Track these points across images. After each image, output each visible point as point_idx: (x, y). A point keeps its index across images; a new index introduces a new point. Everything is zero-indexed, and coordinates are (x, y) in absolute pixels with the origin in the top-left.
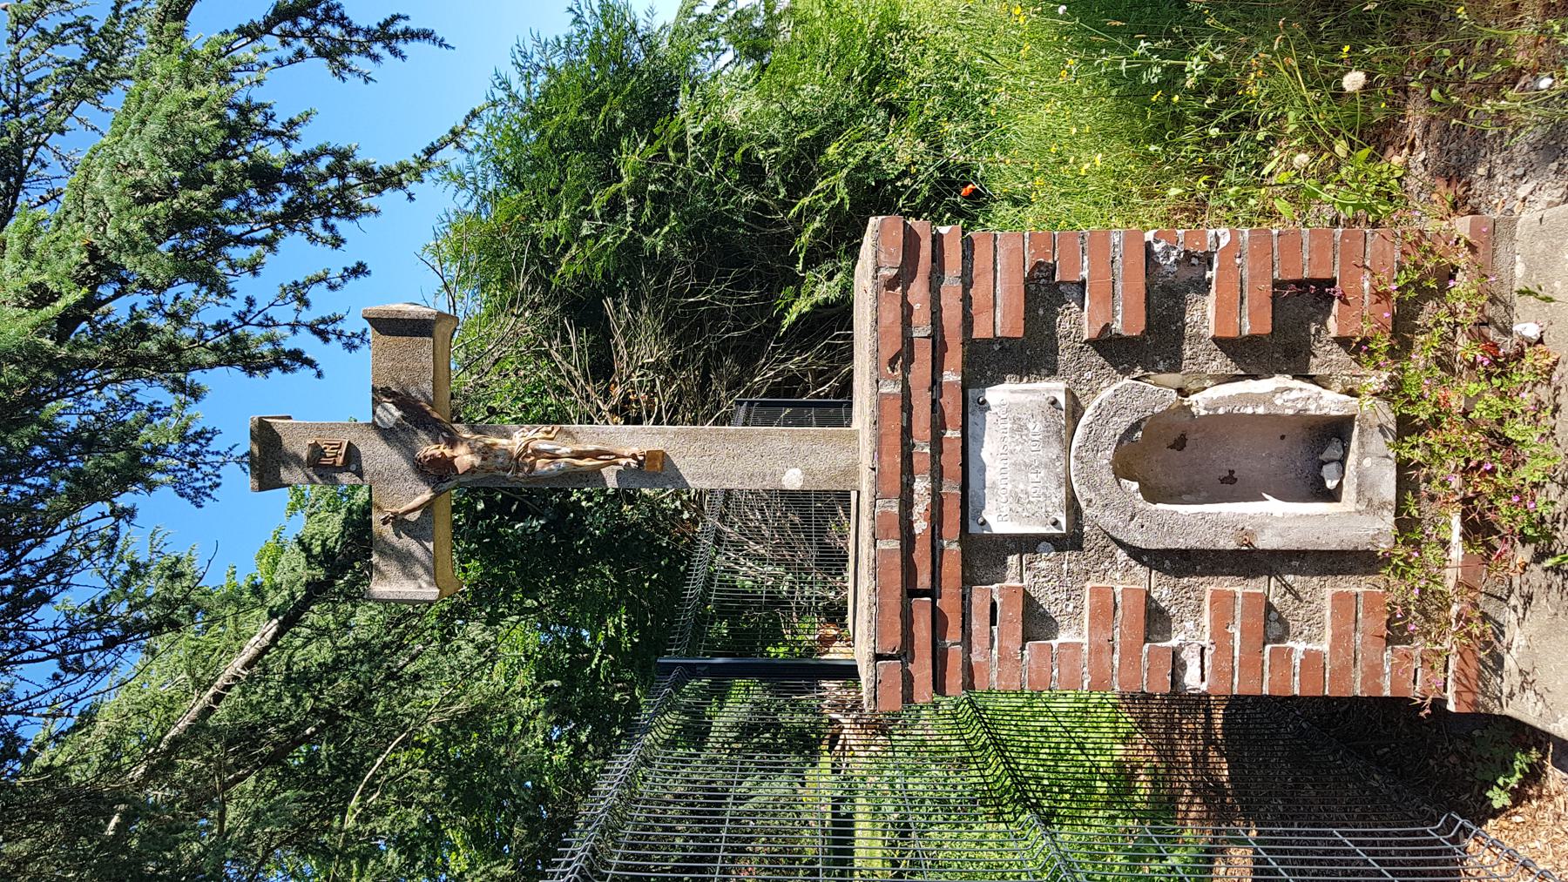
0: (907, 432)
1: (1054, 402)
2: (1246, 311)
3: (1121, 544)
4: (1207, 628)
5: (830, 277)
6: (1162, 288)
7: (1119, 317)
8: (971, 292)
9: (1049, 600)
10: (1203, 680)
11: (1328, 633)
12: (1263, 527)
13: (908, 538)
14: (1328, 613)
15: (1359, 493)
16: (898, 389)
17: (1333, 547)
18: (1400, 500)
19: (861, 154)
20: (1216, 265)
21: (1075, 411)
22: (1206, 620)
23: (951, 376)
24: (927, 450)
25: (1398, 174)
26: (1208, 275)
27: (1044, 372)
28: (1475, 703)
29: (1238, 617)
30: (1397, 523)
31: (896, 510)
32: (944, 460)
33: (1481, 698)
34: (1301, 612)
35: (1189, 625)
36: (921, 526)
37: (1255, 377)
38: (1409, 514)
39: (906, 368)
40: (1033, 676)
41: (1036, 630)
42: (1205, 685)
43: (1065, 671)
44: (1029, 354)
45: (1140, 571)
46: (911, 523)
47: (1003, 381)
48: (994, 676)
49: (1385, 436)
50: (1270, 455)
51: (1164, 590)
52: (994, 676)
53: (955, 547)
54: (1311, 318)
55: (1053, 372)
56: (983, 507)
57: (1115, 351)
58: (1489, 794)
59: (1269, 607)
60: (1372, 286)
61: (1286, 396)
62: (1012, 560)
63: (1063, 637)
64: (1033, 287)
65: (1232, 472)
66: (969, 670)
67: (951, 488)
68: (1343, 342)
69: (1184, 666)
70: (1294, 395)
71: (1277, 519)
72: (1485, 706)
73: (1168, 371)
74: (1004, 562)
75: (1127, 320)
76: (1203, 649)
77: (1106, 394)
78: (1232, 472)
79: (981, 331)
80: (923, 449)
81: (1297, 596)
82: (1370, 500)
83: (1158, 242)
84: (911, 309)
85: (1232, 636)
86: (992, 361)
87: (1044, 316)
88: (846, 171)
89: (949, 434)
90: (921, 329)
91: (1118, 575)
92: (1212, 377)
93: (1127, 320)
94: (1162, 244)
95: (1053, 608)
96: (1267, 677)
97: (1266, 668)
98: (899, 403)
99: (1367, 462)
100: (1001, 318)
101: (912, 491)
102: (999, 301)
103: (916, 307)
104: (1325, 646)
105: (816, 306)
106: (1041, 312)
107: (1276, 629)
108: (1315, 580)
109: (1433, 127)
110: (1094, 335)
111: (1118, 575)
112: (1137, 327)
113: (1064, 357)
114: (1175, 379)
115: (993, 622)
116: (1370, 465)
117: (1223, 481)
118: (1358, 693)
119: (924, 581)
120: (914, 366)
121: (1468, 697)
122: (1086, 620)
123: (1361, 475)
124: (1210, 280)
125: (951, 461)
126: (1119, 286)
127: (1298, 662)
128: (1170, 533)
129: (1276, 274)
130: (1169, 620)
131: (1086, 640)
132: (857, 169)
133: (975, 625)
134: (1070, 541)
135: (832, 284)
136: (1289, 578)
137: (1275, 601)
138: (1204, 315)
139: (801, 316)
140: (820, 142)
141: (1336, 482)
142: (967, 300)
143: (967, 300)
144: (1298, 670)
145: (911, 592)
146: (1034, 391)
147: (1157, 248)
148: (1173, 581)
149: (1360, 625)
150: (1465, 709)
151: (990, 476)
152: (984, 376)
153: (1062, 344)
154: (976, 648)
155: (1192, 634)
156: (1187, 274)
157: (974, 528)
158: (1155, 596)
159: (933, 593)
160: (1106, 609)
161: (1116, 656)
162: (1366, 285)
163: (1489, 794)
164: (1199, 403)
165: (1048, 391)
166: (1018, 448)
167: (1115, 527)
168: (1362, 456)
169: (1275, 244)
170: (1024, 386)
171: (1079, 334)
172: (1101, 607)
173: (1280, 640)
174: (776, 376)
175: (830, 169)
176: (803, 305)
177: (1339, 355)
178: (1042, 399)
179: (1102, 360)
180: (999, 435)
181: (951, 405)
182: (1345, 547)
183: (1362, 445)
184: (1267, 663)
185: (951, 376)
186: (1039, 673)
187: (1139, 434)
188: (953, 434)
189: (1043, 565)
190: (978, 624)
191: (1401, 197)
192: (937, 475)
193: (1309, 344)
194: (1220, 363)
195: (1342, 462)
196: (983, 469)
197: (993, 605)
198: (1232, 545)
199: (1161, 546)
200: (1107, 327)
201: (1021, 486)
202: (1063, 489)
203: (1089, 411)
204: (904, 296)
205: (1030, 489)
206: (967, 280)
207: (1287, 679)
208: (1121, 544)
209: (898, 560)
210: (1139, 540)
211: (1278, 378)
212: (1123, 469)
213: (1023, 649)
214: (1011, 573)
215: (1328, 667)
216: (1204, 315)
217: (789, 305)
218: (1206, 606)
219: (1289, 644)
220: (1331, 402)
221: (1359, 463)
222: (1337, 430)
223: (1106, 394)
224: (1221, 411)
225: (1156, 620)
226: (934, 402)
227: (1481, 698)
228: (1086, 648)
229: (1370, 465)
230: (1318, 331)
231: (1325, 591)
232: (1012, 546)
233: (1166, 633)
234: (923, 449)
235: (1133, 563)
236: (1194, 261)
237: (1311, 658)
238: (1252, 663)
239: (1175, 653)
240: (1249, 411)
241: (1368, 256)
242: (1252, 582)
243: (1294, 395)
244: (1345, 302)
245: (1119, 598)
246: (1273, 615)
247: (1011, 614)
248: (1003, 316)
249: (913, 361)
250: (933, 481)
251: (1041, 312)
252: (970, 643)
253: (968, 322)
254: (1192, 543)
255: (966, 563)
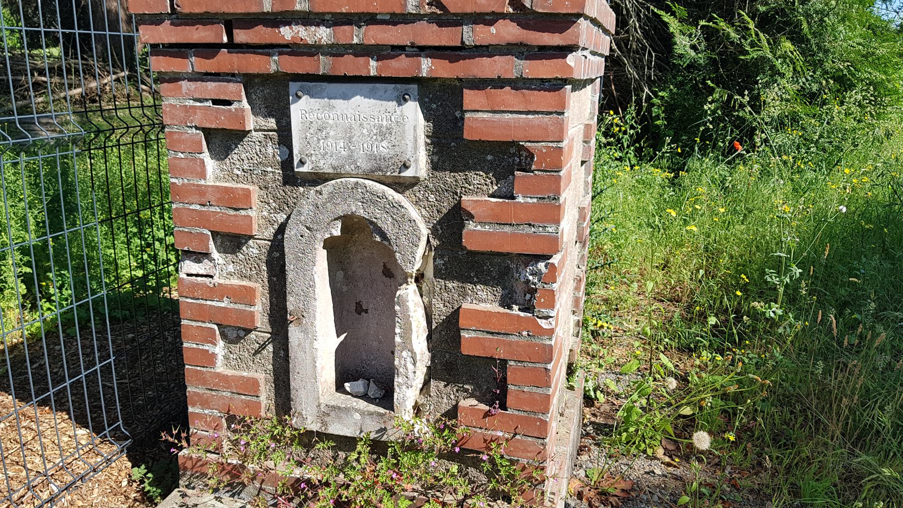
0: (371, 19)
1: (406, 167)
2: (481, 335)
3: (289, 217)
4: (227, 282)
5: (693, 47)
6: (508, 268)
7: (479, 228)
8: (508, 88)
9: (242, 154)
10: (188, 275)
11: (230, 372)
12: (305, 331)
13: (276, 20)
14: (245, 374)
15: (334, 408)
16: (411, 9)
17: (292, 384)
18: (330, 437)
19: (783, 69)
20: (522, 314)
21: (401, 185)
22: (235, 282)
23: (426, 66)
24: (356, 41)
25: (649, 451)
26: (516, 307)
27: (436, 158)
28: (185, 469)
29: (236, 306)
30: (311, 433)
31: (298, 7)
32: (349, 58)
33: (189, 473)
34: (246, 354)
35: (231, 268)
36: (287, 33)
37: (429, 338)
38: (317, 442)
39: (432, 19)
40: (176, 136)
41: (216, 141)
42: (185, 276)
43: (183, 164)
44: (451, 146)
45: (270, 232)
46: (288, 23)
47: (427, 119)
48: (172, 101)
49: (377, 432)
50: (380, 342)
51: (255, 250)
52: (172, 101)
53: (273, 68)
54: (477, 386)
55: (435, 166)
56: (312, 96)
57: (450, 225)
58: (143, 467)
59: (248, 331)
60: (498, 438)
61: (409, 360)
62: (272, 123)
63: (211, 164)
64: (512, 150)
65: (366, 311)
66: (174, 78)
67: (323, 65)
68: (453, 413)
69: (198, 261)
70: (410, 367)
71: (312, 343)
72: (184, 475)
73: (435, 267)
74: (269, 115)
75: (476, 236)
76: (211, 277)
77: (413, 213)
78: (366, 311)
79: (470, 98)
80: (356, 36)
81: (257, 352)
82: (328, 415)
83: (546, 266)
84: (491, 23)
85: (221, 300)
86: (443, 105)
87: (485, 160)
88: (770, 56)
89: (373, 63)
90: (470, 35)
91: (265, 213)
92: (430, 302)
93: (476, 236)
94: (544, 270)
95: (235, 157)
96: (194, 324)
97: (200, 324)
98: (398, 11)
99: (357, 416)
100: (483, 118)
101: (318, 25)
102: (498, 116)
103: (493, 30)
104: (221, 367)
105: (672, 36)
106: (489, 157)
107: (232, 334)
108: (270, 367)
109: (678, 483)
110: (464, 205)
111: (265, 213)
112: (469, 243)
113: (449, 177)
114: (430, 272)
115: (216, 102)
116: (356, 417)
117: (359, 305)
118: (189, 389)
119: (241, 36)
120: (435, 27)
121: (189, 464)
122: (226, 185)
123: (347, 410)
124: (510, 308)
125: (349, 65)
126: (507, 229)
127: (207, 348)
128: (298, 259)
129: (512, 363)
130: (233, 252)
131: (210, 182)
132: (773, 67)
133: (211, 85)
134: (291, 176)
135: (688, 48)
136: (270, 348)
137: (252, 335)
138: (482, 301)
139: (666, 25)
140: (797, 38)
141: (348, 389)
142: (499, 83)
143: (499, 83)
144: (201, 347)
145: (231, 23)
146: (416, 148)
147: (541, 265)
148: (264, 258)
149: (236, 396)
150: (180, 461)
151: (339, 103)
152: (432, 101)
153: (460, 176)
154: (192, 85)
155: (221, 268)
156: (519, 288)
157: (293, 87)
158: (251, 242)
159: (232, 46)
160: (236, 201)
161: (198, 207)
162: (500, 434)
163: (143, 467)
164: (409, 293)
165: (416, 161)
166: (365, 131)
167: (300, 213)
168: (362, 413)
169: (538, 365)
170: (422, 139)
171: (466, 193)
172: (235, 197)
173: (224, 336)
174: (627, 10)
175: (774, 44)
176: (674, 25)
177: (446, 406)
178: (409, 154)
179: (445, 211)
180: (376, 114)
181: (400, 66)
182: (293, 392)
183: (371, 414)
184: (204, 325)
185: (426, 66)
186: (180, 141)
187: (378, 239)
188: (373, 67)
189: (270, 150)
190: (212, 88)
191: (628, 451)
192: (336, 50)
193: (455, 382)
194: (441, 310)
195: (365, 397)
196: (346, 97)
197: (228, 103)
198: (290, 307)
199: (286, 250)
200: (471, 217)
201: (332, 133)
202: (331, 171)
203: (398, 197)
204: (504, 16)
205: (330, 141)
206: (519, 84)
207: (193, 339)
208: (289, 217)
209: (254, 9)
210: (290, 233)
211: (428, 355)
212: (350, 223)
213: (197, 128)
214: (261, 121)
215: (205, 369)
216: (481, 301)
217: (673, 14)
218: (245, 283)
219: (221, 343)
220: (407, 393)
221: (357, 410)
222: (385, 397)
223: (413, 213)
224: (397, 308)
225: (232, 242)
226: (402, 48)
227: (189, 473)
228: (202, 182)
229: (356, 417)
230: (466, 391)
231: (261, 374)
232: (284, 123)
233: (223, 249)
234: (356, 36)
235: (276, 227)
236: (528, 296)
237: (210, 359)
238: (203, 314)
239: (207, 255)
240: (397, 330)
241: (524, 438)
242: (266, 319)
243: (410, 367)
244: (487, 414)
245: (243, 213)
246: (242, 333)
247: (220, 119)
248: (484, 120)
249: (440, 25)
250: (332, 46)
251: (489, 157)
252: (196, 80)
253: (480, 84)
254: (290, 276)
255: (266, 79)
